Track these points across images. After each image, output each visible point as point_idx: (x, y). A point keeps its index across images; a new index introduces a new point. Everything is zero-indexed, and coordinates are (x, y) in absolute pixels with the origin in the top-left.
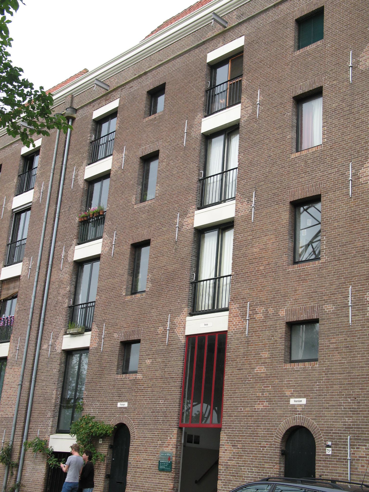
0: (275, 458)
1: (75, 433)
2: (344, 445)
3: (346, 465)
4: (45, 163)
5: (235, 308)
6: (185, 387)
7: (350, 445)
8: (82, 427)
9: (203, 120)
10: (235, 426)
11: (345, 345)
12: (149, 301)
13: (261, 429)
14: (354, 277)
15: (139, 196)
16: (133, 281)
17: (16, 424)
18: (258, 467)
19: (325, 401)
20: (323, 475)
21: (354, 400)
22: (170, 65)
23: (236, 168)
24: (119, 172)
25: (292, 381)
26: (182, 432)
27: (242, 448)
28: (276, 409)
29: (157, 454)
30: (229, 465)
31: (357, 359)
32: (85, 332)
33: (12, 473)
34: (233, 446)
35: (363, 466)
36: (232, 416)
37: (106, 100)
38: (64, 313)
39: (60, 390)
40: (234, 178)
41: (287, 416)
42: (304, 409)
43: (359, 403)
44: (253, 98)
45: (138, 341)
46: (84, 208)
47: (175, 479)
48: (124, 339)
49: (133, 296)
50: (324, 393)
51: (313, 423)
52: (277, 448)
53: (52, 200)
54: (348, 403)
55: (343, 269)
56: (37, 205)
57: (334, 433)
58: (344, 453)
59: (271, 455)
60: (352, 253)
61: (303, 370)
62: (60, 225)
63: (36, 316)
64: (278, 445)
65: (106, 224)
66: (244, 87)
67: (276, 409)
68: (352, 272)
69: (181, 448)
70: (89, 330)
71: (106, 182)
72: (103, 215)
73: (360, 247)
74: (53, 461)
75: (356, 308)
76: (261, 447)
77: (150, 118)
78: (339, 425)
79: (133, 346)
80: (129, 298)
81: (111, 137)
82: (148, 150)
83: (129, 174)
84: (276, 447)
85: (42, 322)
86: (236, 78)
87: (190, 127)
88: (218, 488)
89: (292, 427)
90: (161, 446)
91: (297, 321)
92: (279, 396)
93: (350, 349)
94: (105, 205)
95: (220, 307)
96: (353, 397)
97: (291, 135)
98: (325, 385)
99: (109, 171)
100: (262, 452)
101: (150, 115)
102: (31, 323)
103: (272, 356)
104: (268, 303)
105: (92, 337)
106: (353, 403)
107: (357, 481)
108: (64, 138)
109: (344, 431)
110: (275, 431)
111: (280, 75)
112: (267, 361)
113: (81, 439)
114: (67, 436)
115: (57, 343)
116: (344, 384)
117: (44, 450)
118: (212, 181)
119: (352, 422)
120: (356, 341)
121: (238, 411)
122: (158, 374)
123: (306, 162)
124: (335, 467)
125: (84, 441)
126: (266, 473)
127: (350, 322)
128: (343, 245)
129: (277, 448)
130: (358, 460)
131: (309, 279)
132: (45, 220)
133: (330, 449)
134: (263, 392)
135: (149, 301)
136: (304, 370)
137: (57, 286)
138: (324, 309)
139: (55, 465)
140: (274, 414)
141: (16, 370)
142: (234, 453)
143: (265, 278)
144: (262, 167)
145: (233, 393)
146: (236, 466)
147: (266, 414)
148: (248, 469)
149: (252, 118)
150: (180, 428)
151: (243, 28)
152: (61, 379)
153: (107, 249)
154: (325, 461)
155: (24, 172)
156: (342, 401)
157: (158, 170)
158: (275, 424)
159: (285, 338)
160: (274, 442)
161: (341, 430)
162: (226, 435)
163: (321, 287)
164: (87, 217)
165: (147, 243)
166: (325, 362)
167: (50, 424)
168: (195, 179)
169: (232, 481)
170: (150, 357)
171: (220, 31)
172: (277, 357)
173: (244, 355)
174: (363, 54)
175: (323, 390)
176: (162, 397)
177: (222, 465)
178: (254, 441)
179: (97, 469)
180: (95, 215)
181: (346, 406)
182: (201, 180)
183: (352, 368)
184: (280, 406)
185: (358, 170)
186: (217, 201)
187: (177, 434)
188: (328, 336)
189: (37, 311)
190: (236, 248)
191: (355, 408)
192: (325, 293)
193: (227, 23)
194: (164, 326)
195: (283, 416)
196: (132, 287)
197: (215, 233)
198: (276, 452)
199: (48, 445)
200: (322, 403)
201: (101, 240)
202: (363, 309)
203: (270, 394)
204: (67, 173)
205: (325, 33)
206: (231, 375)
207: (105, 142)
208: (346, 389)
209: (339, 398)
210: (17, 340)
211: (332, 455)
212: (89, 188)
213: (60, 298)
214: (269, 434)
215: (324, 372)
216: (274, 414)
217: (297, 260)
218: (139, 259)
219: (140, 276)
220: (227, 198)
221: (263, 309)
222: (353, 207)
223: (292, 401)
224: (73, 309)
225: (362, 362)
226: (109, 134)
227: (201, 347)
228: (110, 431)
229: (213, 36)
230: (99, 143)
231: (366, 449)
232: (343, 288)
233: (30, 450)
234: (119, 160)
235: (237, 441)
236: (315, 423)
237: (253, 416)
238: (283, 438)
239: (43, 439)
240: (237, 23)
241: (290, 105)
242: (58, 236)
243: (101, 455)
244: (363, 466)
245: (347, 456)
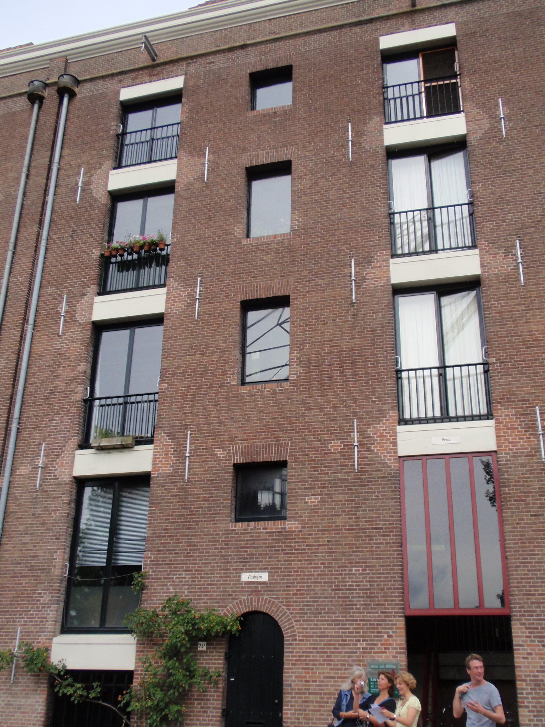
12: (301, 397)
22: (300, 41)
32: (136, 445)
38: (73, 410)
39: (68, 550)
48: (240, 459)
83: (222, 191)
85: (14, 427)
105: (155, 455)
115: (57, 464)
176: (359, 563)
177: (525, 681)
179: (197, 700)
241: (241, 179)
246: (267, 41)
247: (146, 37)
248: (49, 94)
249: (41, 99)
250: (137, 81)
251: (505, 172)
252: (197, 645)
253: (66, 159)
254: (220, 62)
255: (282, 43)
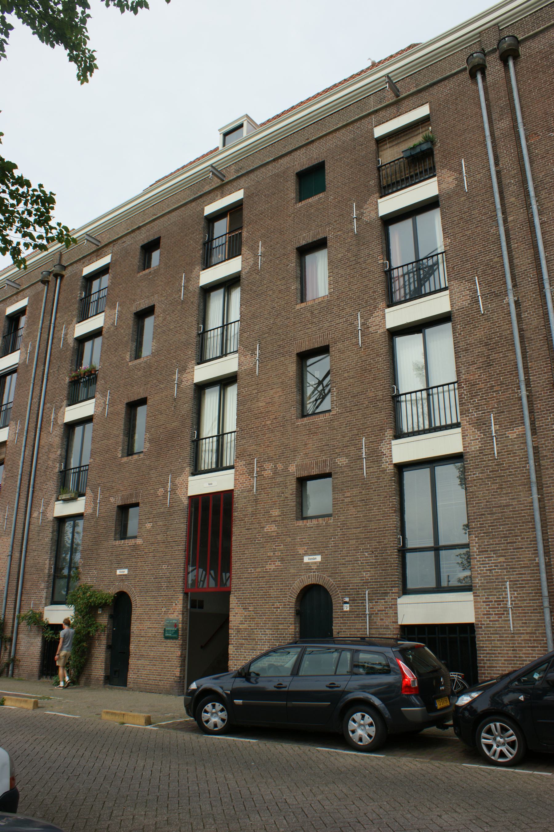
0: (290, 618)
1: (72, 604)
2: (363, 600)
3: (364, 620)
4: (32, 323)
5: (241, 466)
6: (190, 550)
7: (369, 600)
8: (80, 597)
9: (201, 272)
10: (245, 588)
11: (360, 498)
12: (147, 462)
13: (274, 589)
14: (367, 428)
15: (134, 352)
16: (129, 442)
17: (7, 597)
18: (271, 629)
19: (341, 556)
20: (341, 632)
21: (371, 554)
22: (165, 219)
23: (238, 321)
24: (112, 329)
25: (305, 538)
26: (188, 598)
27: (254, 611)
28: (289, 568)
29: (162, 621)
30: (241, 629)
31: (374, 512)
33: (6, 647)
34: (243, 609)
35: (382, 619)
36: (242, 578)
37: (97, 256)
40: (236, 332)
41: (301, 575)
42: (319, 566)
43: (377, 556)
44: (254, 249)
45: (137, 505)
46: (74, 367)
47: (183, 646)
48: (120, 503)
49: (130, 457)
50: (340, 548)
51: (329, 580)
52: (292, 608)
53: (39, 360)
54: (366, 557)
55: (356, 420)
56: (23, 366)
57: (351, 589)
58: (362, 609)
59: (285, 615)
60: (365, 403)
61: (317, 527)
62: (48, 386)
63: (25, 482)
64: (292, 605)
65: (98, 383)
66: (244, 239)
67: (289, 568)
68: (365, 423)
69: (187, 614)
70: (83, 495)
71: (98, 341)
72: (95, 374)
73: (373, 397)
74: (49, 634)
75: (370, 460)
76: (274, 608)
77: (144, 272)
78: (357, 580)
79: (131, 510)
80: (125, 459)
81: (103, 293)
82: (143, 305)
83: (122, 331)
84: (290, 608)
85: (31, 489)
86: (236, 230)
87: (188, 280)
88: (229, 653)
89: (306, 586)
90: (166, 613)
91: (308, 476)
92: (291, 555)
93: (365, 502)
94: (97, 363)
95: (224, 465)
96: (370, 551)
97: (295, 286)
98: (341, 540)
99: (102, 328)
100: (275, 613)
101: (144, 270)
102: (20, 490)
103: (283, 514)
104: (277, 459)
106: (370, 557)
107: (376, 634)
108: (52, 296)
109: (361, 586)
110: (289, 591)
111: (282, 226)
112: (277, 519)
113: (79, 610)
114: (63, 607)
116: (361, 538)
117: (38, 622)
118: (212, 335)
119: (369, 577)
120: (371, 494)
121: (248, 573)
122: (159, 537)
123: (312, 313)
124: (354, 623)
125: (82, 611)
126: (281, 634)
127: (365, 475)
128: (354, 396)
129: (292, 608)
130: (377, 614)
131: (319, 432)
132: (32, 381)
133: (348, 605)
134: (274, 551)
135: (147, 462)
136: (318, 526)
137: (47, 450)
138: (337, 463)
139: (52, 638)
140: (287, 573)
141: (5, 540)
142: (245, 616)
143: (272, 432)
144: (266, 319)
145: (242, 554)
146: (248, 629)
147: (279, 574)
148: (261, 632)
149: (254, 269)
150: (186, 594)
151: (242, 181)
152: (54, 548)
153: (100, 409)
154: (343, 617)
155: (9, 333)
156: (359, 555)
157: (154, 326)
158: (289, 583)
159: (296, 494)
160: (288, 602)
161: (358, 586)
162: (237, 598)
163: (333, 439)
164: (77, 376)
165: (143, 402)
166: (340, 516)
167: (44, 595)
168: (194, 333)
169: (244, 644)
170: (150, 520)
171: (217, 185)
172: (288, 515)
173: (253, 514)
174: (366, 206)
175: (338, 546)
176: (165, 562)
177: (233, 629)
178: (267, 603)
180: (86, 374)
181: (363, 560)
182: (201, 334)
183: (368, 521)
184: (293, 565)
185: (366, 320)
186: (218, 355)
187: (183, 600)
188: (342, 490)
189: (26, 478)
190: (240, 403)
191: (373, 562)
192: (338, 446)
193: (225, 177)
194: (165, 487)
195: (297, 575)
196: (128, 448)
197: (217, 388)
198: (290, 613)
199: (43, 617)
200: (338, 559)
201: (94, 400)
202: (377, 461)
203: (283, 553)
204: (56, 332)
205: (327, 186)
206: (239, 535)
207: (96, 299)
208: (363, 544)
209: (356, 553)
210: (5, 508)
211: (350, 611)
212: (79, 347)
213: (50, 463)
214: (282, 594)
215: (339, 527)
216: (287, 573)
217: (305, 414)
218: (135, 419)
219: (137, 437)
220: (228, 352)
221: (271, 465)
222: (363, 357)
223: (306, 559)
224: (64, 474)
225: (378, 515)
226: (100, 291)
227: (206, 508)
228: (109, 601)
229: (210, 189)
230: (90, 300)
231: (385, 602)
232: (356, 440)
233: (23, 624)
234: (112, 317)
235: (248, 603)
236: (331, 580)
237: (265, 577)
238: (297, 598)
239: (37, 611)
240: (235, 177)
241: (293, 257)
242: (47, 397)
243: (101, 625)
244: (382, 619)
245: (366, 611)
246: (149, 222)
247: (388, 77)
248: (51, 278)
249: (48, 282)
250: (91, 261)
251: (257, 295)
252: (97, 610)
253: (58, 319)
254: (271, 170)
255: (157, 222)
